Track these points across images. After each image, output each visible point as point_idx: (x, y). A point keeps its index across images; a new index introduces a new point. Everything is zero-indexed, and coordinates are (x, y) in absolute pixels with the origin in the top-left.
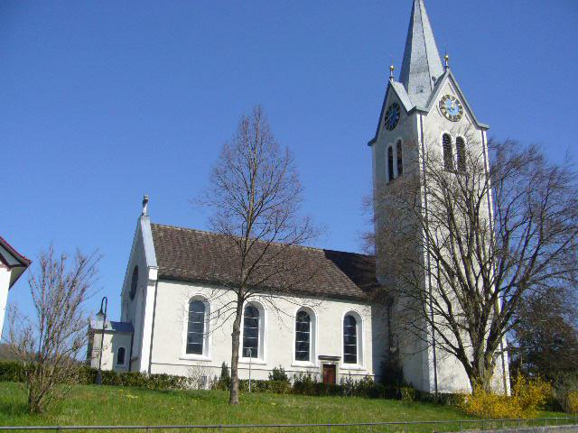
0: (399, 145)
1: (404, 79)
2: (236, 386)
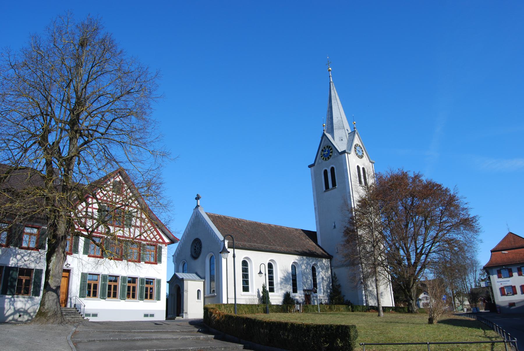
0: (332, 169)
1: (332, 132)
2: (381, 309)
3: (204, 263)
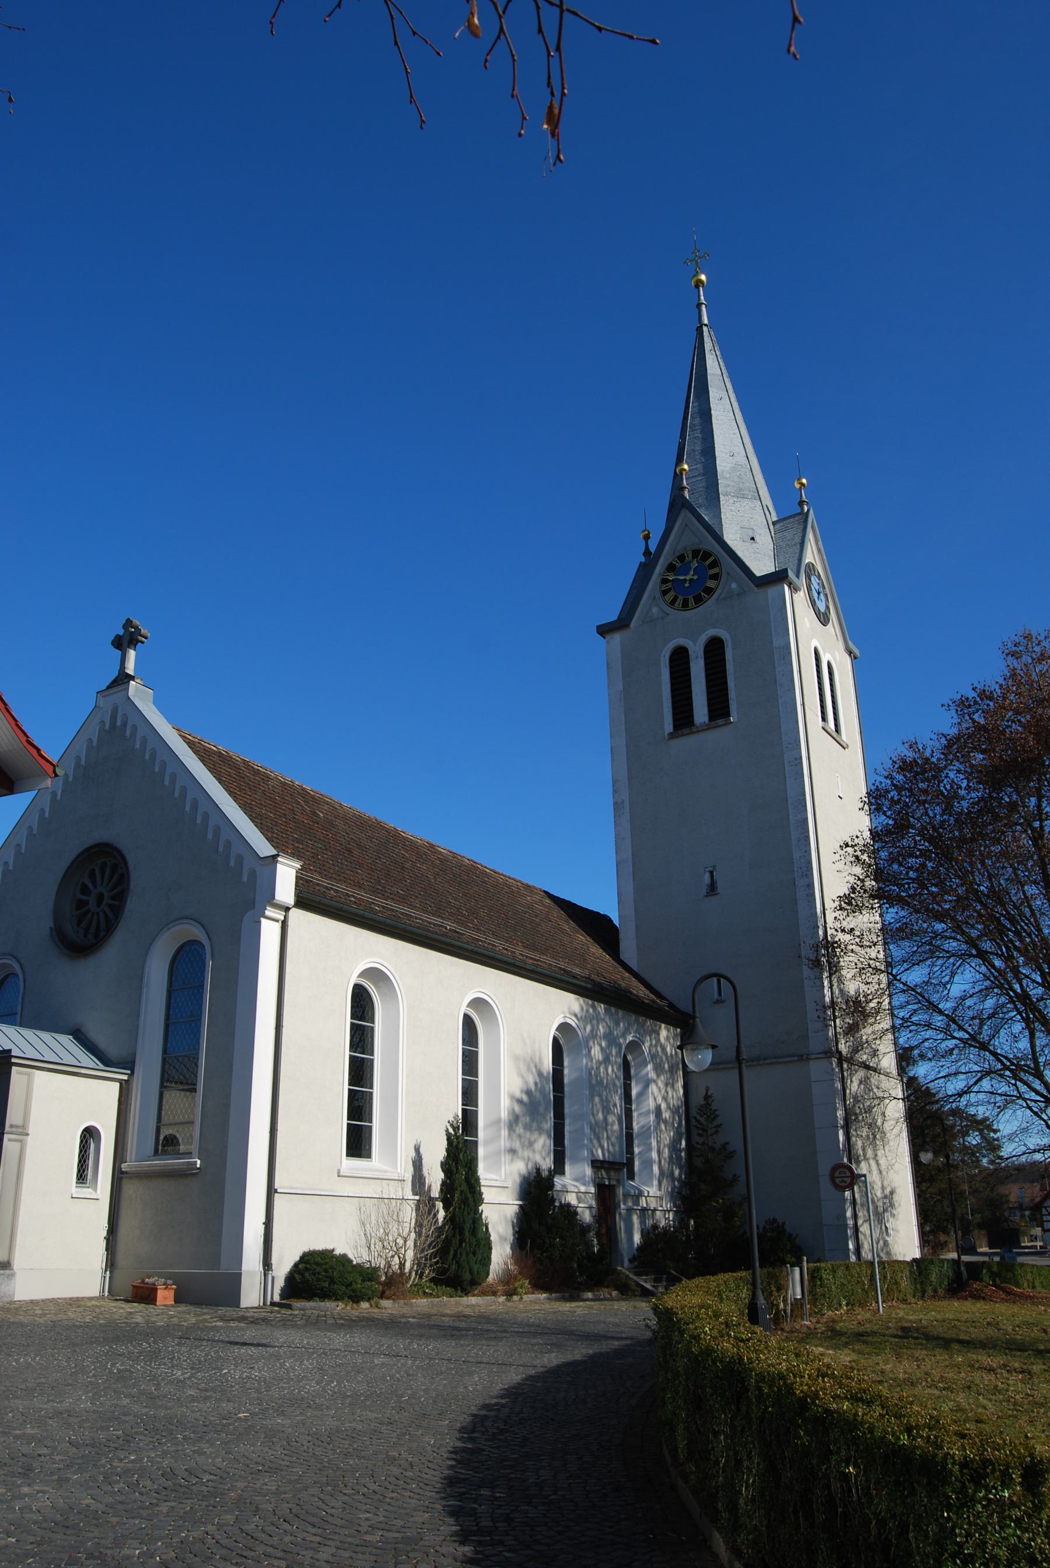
0: (715, 649)
3: (137, 979)
